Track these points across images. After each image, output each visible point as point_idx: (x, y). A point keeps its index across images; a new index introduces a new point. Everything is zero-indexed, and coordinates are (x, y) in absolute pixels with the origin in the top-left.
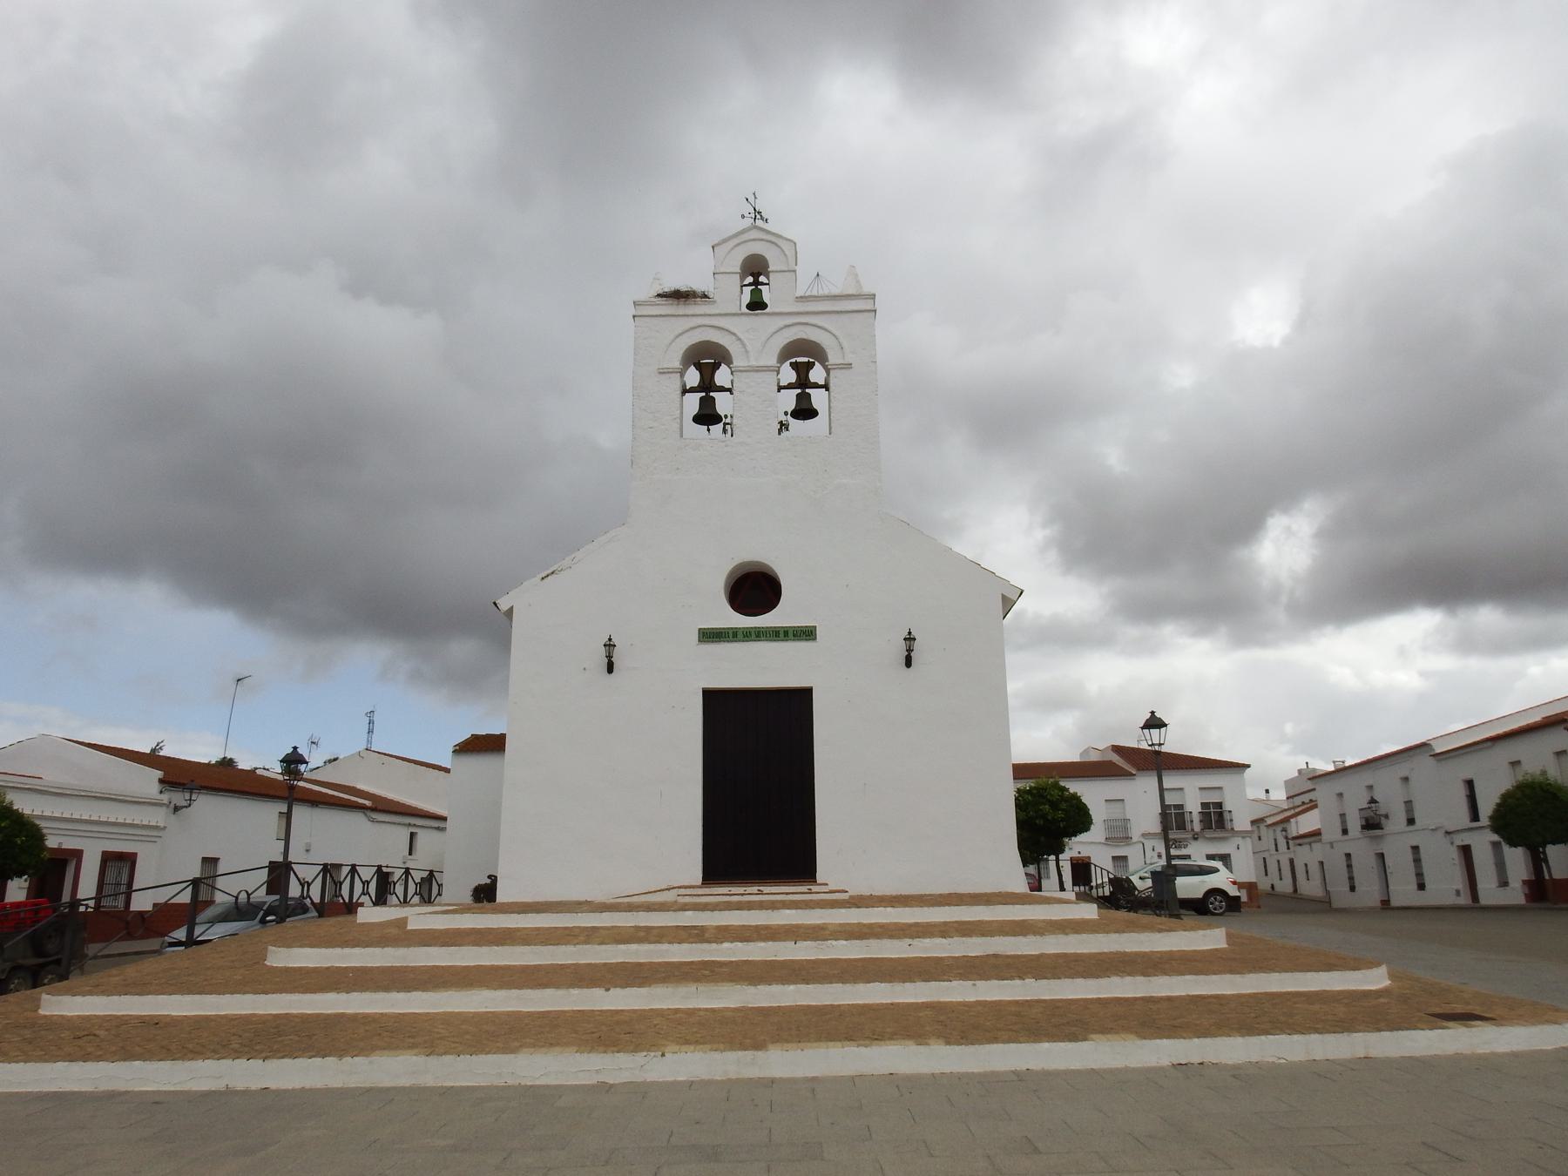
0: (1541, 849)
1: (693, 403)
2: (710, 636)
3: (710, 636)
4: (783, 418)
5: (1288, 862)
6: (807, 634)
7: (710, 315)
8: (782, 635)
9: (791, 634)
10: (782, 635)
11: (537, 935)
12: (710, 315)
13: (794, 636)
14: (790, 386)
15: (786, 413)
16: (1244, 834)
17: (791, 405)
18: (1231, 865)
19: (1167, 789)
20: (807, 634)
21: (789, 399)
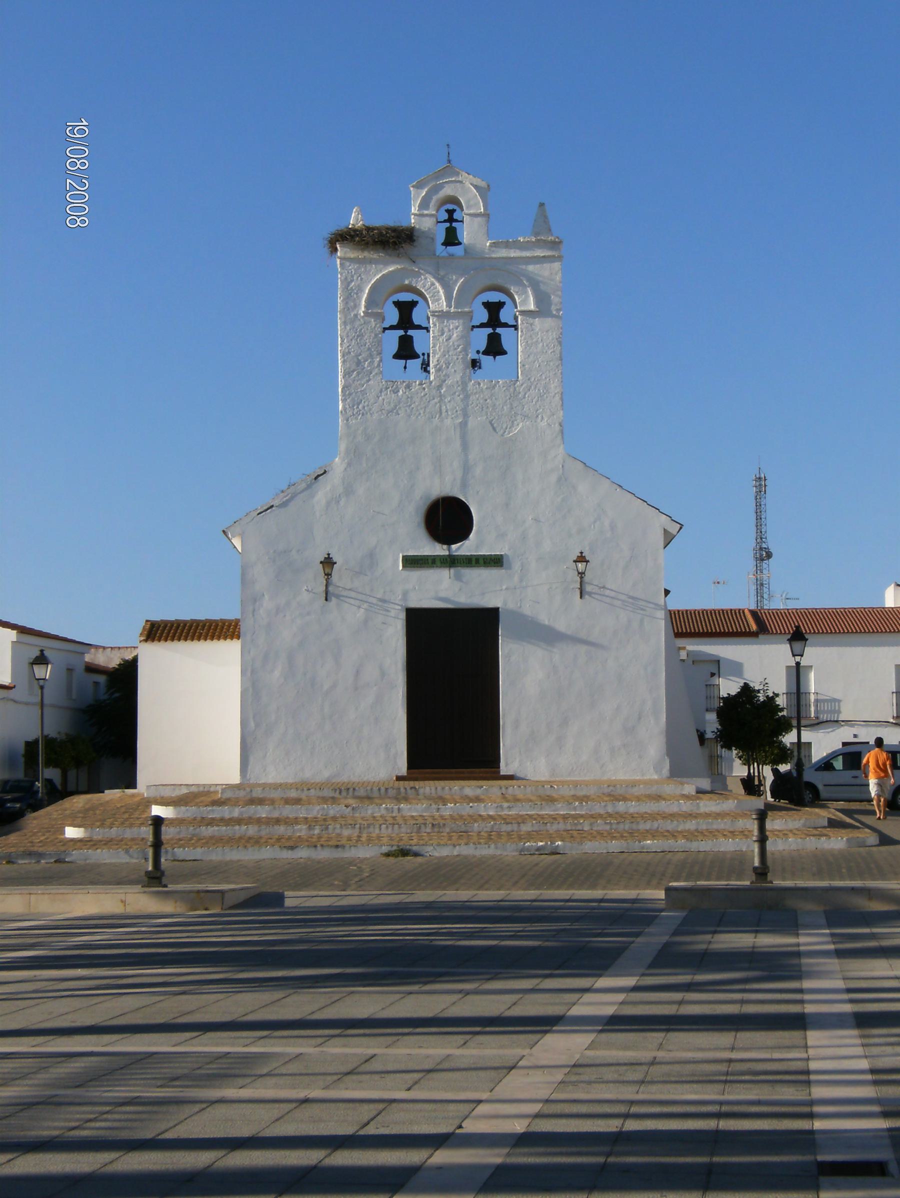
0: (784, 734)
1: (392, 339)
2: (411, 562)
3: (411, 562)
4: (476, 357)
5: (417, 575)
6: (496, 561)
7: (857, 785)
8: (474, 562)
9: (481, 561)
10: (474, 562)
11: (115, 815)
12: (857, 785)
13: (485, 563)
14: (482, 325)
15: (478, 352)
16: (341, 831)
17: (483, 345)
18: (819, 770)
19: (406, 362)
20: (496, 561)
21: (481, 338)
